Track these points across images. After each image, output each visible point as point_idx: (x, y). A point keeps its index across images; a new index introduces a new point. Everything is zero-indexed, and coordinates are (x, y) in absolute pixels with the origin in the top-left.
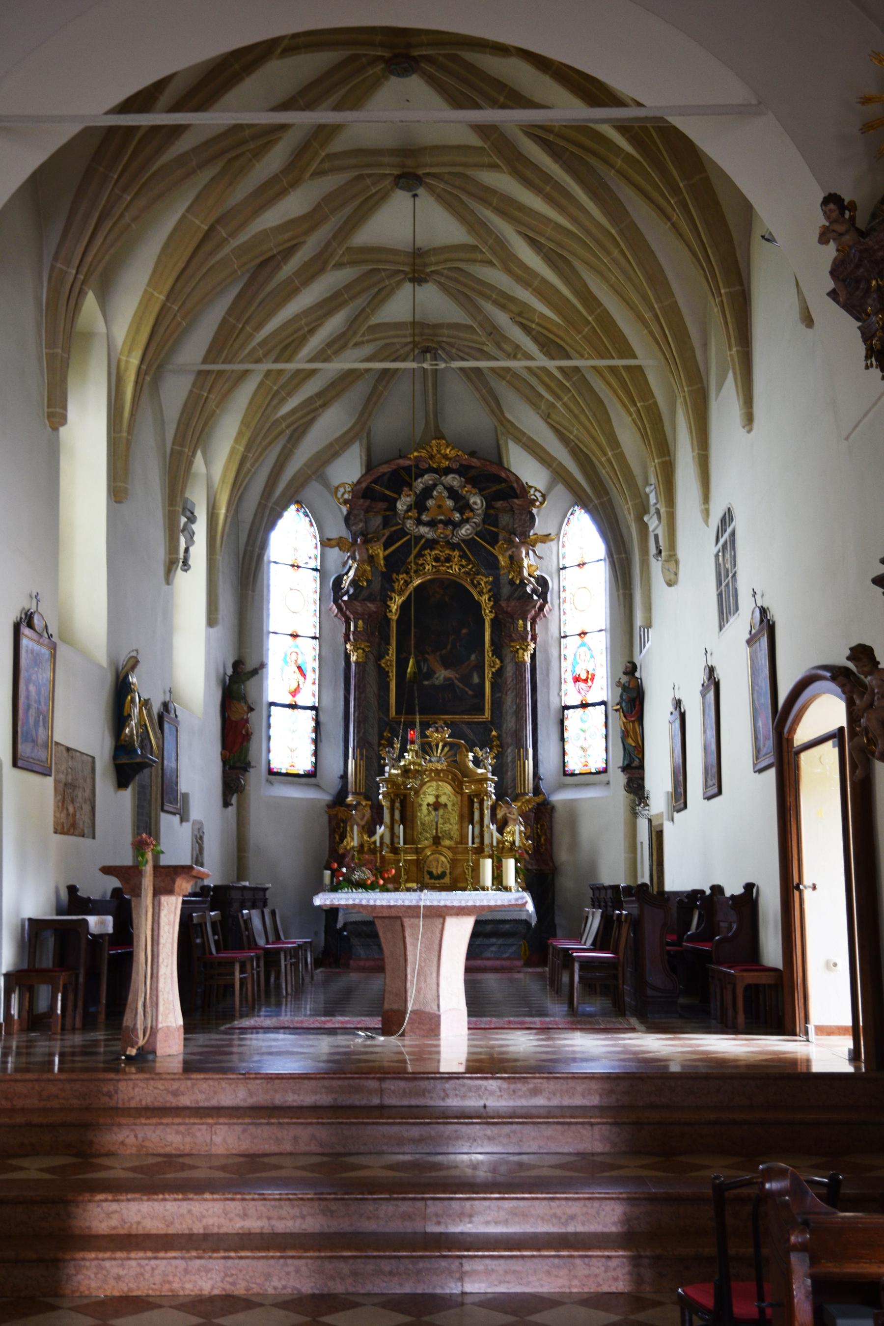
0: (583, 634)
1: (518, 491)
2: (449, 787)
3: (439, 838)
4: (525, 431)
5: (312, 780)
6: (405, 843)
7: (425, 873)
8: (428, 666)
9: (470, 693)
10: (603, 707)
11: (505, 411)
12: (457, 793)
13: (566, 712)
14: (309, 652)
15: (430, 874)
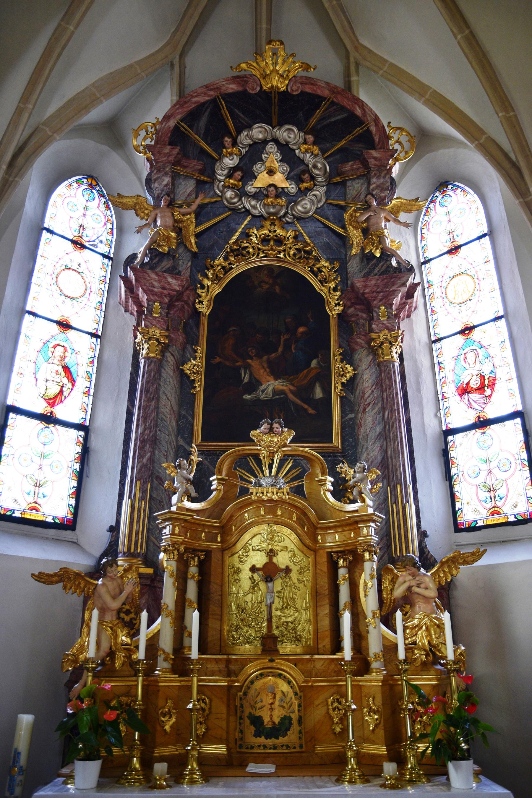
0: (467, 330)
1: (377, 139)
2: (293, 536)
3: (274, 639)
4: (386, 57)
5: (68, 534)
6: (202, 650)
7: (247, 722)
8: (251, 375)
9: (311, 411)
10: (518, 420)
11: (359, 38)
12: (308, 547)
13: (450, 438)
14: (82, 351)
15: (257, 721)
